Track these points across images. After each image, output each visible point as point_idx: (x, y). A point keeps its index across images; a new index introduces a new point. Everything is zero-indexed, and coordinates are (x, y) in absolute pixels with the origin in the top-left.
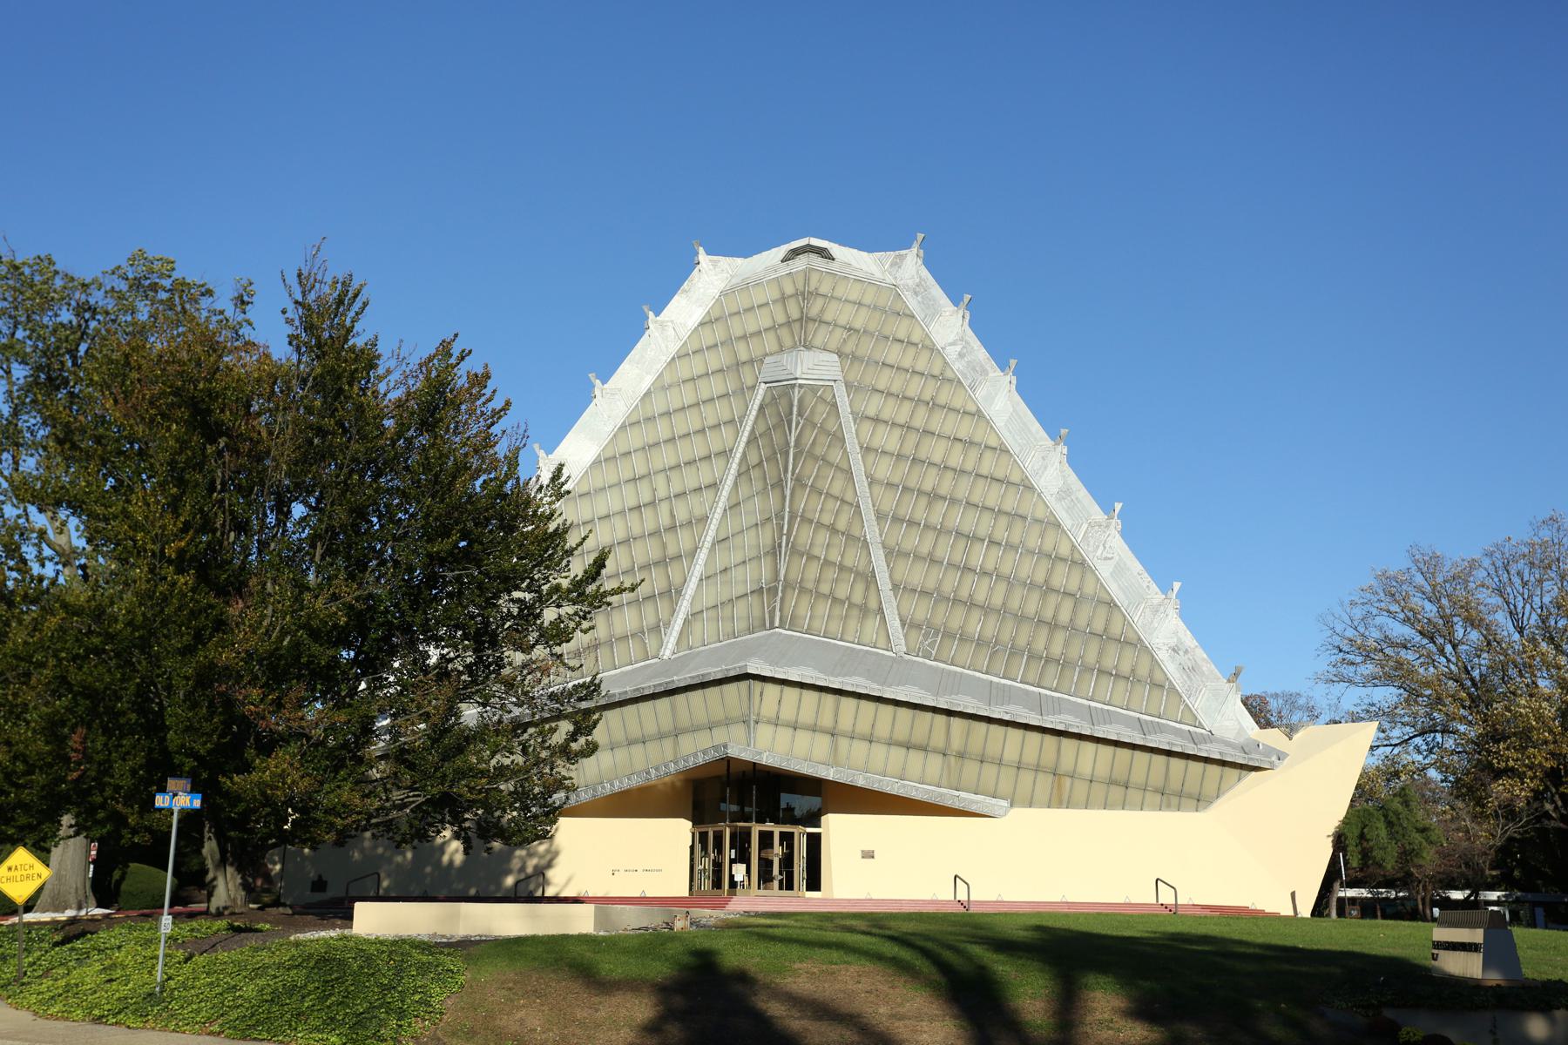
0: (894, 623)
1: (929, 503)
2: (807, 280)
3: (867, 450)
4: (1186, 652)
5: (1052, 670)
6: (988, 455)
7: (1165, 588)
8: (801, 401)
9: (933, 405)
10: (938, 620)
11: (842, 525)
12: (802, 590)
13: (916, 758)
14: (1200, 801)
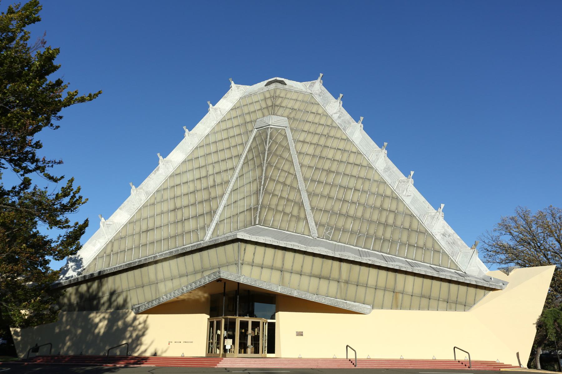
0: (312, 224)
1: (327, 174)
2: (275, 92)
3: (299, 153)
4: (449, 236)
5: (386, 244)
6: (352, 155)
7: (436, 207)
8: (271, 133)
9: (328, 136)
10: (333, 223)
11: (288, 182)
12: (270, 209)
13: (324, 283)
14: (466, 306)
